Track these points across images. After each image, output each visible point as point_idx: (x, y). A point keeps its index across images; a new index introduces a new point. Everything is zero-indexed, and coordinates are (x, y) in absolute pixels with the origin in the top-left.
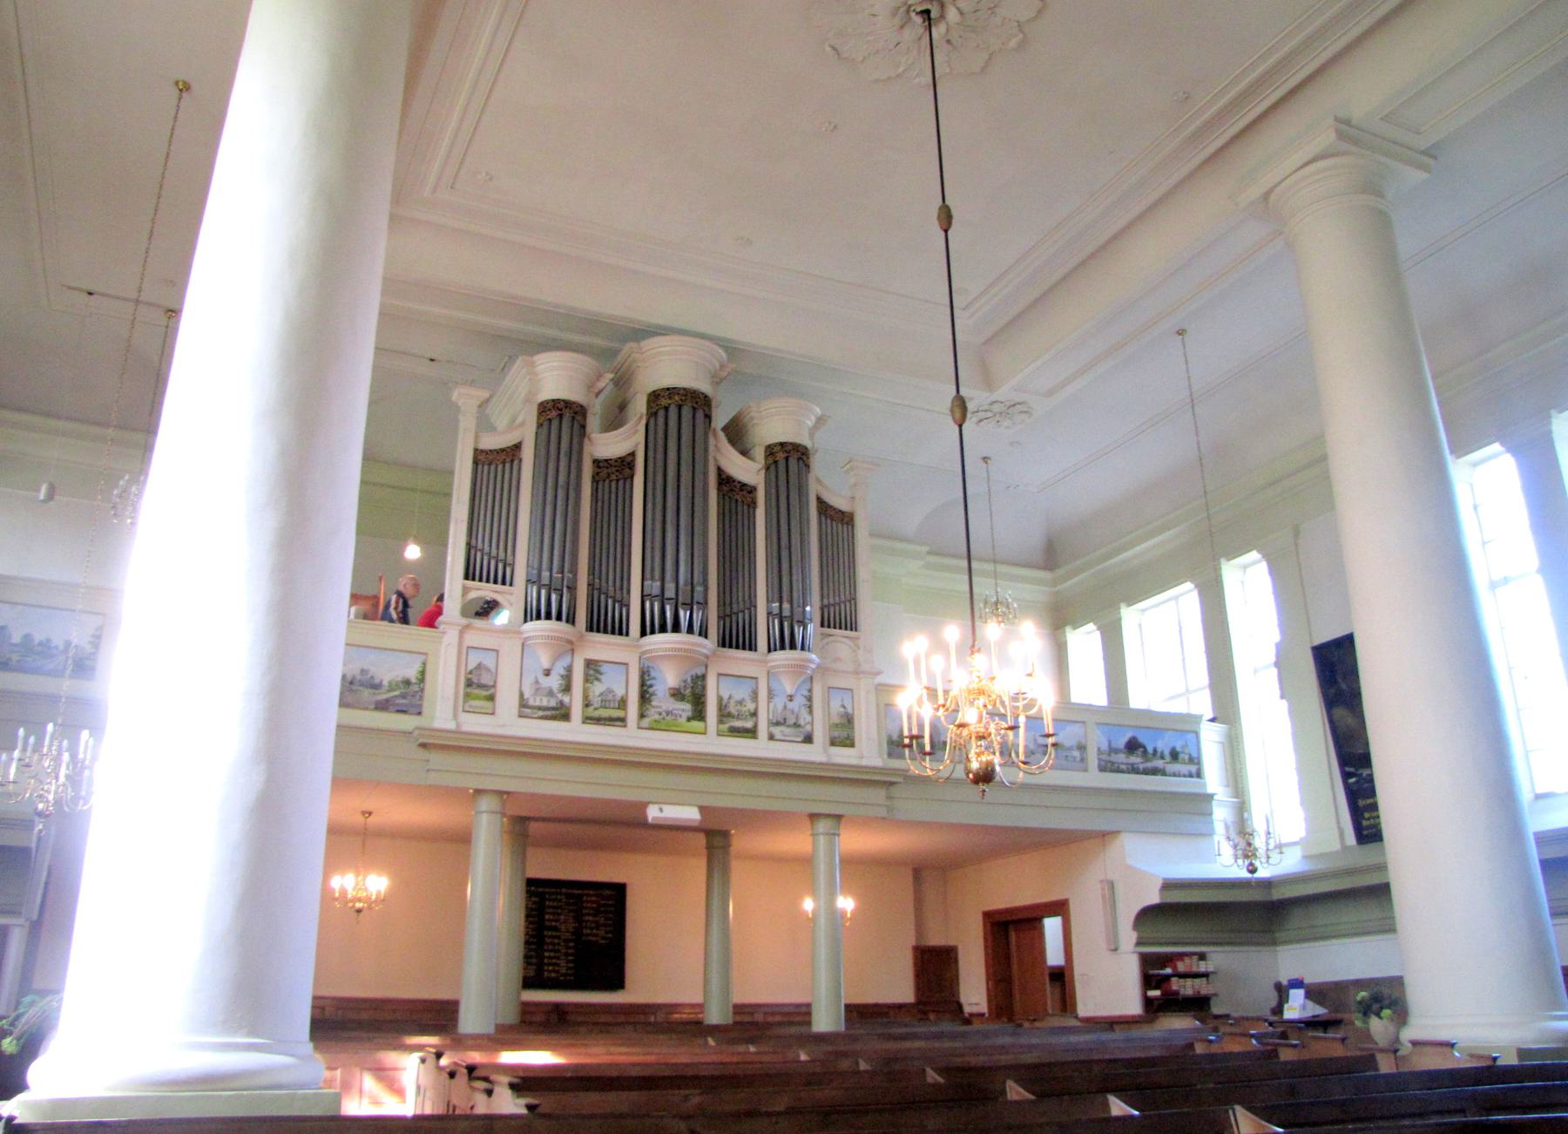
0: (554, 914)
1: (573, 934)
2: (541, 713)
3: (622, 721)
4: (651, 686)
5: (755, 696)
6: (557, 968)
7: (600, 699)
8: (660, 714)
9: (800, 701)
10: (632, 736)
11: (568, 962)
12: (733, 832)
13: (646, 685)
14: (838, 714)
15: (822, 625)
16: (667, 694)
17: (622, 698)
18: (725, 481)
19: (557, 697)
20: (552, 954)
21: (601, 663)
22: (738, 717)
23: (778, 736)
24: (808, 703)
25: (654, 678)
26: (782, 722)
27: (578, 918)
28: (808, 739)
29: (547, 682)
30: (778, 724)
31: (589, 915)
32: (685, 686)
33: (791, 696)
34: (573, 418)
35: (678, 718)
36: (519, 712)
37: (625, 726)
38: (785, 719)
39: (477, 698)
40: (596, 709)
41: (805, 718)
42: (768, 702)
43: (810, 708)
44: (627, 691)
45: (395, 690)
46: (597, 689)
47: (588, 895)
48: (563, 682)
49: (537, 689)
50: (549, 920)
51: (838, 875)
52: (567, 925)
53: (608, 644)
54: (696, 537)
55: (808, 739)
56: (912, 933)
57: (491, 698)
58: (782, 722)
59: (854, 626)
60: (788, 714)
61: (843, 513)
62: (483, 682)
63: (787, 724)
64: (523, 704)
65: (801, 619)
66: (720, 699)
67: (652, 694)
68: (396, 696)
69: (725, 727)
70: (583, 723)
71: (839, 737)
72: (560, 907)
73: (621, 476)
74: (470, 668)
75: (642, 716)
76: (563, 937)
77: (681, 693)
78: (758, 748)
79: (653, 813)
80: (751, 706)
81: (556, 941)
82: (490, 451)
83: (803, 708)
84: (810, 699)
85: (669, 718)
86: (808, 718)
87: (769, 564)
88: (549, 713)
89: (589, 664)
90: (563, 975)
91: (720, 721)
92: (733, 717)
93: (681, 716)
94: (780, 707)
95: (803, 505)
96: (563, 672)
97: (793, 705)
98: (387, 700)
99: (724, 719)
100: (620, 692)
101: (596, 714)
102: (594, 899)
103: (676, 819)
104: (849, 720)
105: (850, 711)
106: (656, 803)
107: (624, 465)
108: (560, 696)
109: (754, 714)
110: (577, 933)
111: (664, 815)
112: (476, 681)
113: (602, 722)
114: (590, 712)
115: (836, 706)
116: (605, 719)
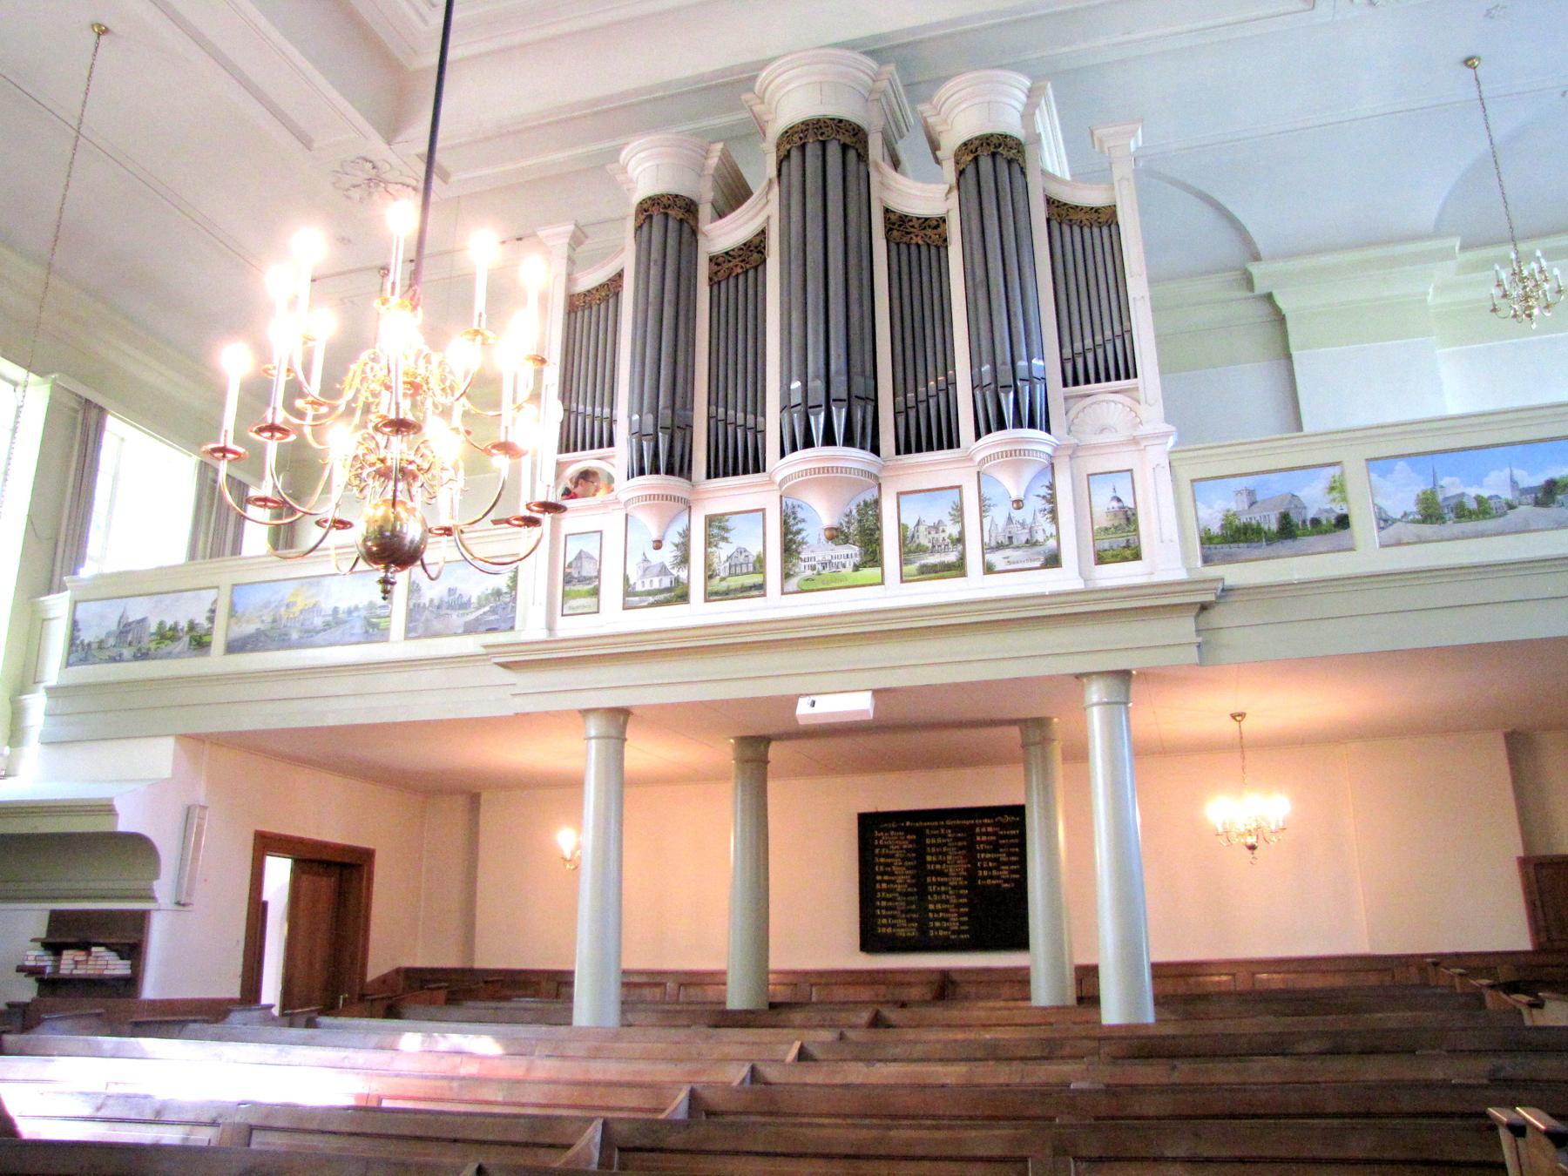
0: (937, 854)
1: (965, 878)
2: (651, 599)
3: (760, 588)
4: (799, 532)
5: (959, 513)
6: (945, 924)
7: (727, 564)
8: (813, 568)
9: (1035, 504)
10: (776, 605)
11: (960, 915)
12: (1056, 720)
13: (791, 533)
14: (1108, 512)
15: (1065, 385)
16: (823, 538)
17: (758, 556)
18: (898, 224)
19: (671, 574)
20: (939, 906)
21: (727, 517)
23: (1000, 565)
24: (1048, 506)
25: (803, 521)
26: (1006, 542)
27: (971, 856)
28: (1053, 561)
29: (656, 557)
30: (1000, 546)
31: (985, 851)
32: (848, 522)
34: (666, 215)
35: (841, 569)
37: (764, 595)
38: (1010, 538)
39: (579, 595)
40: (723, 579)
41: (1044, 526)
42: (981, 517)
43: (1053, 514)
44: (999, 572)
45: (484, 606)
46: (724, 551)
47: (981, 826)
48: (679, 553)
49: (645, 570)
50: (931, 863)
51: (1128, 770)
52: (956, 868)
53: (742, 487)
54: (682, 280)
55: (1053, 561)
56: (1518, 840)
57: (595, 592)
58: (1006, 542)
59: (1131, 371)
61: (1097, 210)
62: (584, 573)
64: (628, 591)
66: (902, 528)
67: (803, 543)
68: (485, 613)
69: (912, 568)
70: (706, 601)
71: (1112, 548)
72: (946, 844)
73: (748, 266)
75: (786, 576)
76: (899, 890)
77: (842, 532)
78: (973, 587)
79: (803, 708)
80: (953, 530)
81: (943, 889)
82: (589, 291)
83: (1039, 516)
84: (1051, 499)
85: (827, 571)
86: (1051, 529)
87: (1462, 422)
88: (661, 597)
89: (710, 521)
90: (954, 932)
91: (904, 562)
92: (925, 552)
93: (844, 566)
94: (1001, 521)
95: (1021, 213)
96: (677, 540)
97: (1023, 515)
98: (477, 619)
99: (912, 556)
100: (755, 549)
101: (723, 586)
102: (990, 829)
104: (1129, 518)
105: (1128, 503)
106: (807, 695)
107: (755, 249)
108: (674, 572)
109: (960, 540)
110: (972, 876)
111: (817, 709)
113: (731, 596)
114: (716, 584)
115: (1103, 503)
116: (736, 590)
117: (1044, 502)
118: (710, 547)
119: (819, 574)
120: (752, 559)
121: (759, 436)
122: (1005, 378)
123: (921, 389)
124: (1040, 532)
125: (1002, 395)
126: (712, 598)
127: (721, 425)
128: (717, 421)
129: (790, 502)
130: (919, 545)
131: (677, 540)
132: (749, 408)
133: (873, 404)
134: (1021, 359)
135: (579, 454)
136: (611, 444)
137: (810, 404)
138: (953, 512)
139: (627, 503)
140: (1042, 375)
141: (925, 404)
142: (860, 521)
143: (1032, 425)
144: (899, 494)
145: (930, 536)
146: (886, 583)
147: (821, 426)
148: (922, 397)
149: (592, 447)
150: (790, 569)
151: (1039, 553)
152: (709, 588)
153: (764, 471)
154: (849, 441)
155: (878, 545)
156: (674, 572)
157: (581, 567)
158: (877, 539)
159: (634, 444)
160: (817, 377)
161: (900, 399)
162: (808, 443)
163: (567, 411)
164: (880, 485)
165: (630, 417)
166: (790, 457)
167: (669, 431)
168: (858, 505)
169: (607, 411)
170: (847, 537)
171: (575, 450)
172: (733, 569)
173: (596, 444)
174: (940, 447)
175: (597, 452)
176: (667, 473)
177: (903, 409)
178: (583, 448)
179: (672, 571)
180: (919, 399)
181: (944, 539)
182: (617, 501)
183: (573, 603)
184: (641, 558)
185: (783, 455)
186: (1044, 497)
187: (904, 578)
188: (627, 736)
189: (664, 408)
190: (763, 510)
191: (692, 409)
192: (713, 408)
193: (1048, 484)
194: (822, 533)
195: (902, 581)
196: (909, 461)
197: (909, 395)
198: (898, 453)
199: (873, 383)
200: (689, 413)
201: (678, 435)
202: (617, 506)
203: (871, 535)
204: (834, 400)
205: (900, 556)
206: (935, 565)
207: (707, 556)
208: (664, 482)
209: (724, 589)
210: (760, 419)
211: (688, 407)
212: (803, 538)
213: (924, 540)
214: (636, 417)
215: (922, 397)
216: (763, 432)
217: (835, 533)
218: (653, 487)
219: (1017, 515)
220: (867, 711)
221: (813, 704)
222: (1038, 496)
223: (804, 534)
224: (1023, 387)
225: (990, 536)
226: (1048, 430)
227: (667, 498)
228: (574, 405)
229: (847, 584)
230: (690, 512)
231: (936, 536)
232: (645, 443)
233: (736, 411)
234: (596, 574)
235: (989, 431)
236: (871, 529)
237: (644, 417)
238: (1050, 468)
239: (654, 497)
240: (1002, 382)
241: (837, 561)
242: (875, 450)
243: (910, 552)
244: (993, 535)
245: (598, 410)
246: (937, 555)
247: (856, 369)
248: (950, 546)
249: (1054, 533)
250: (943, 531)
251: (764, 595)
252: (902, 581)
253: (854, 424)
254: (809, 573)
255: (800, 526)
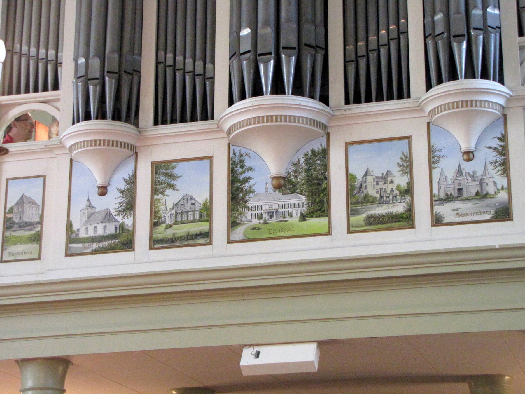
2: (95, 246)
4: (246, 180)
7: (173, 212)
8: (260, 217)
12: (507, 378)
13: (239, 181)
16: (270, 186)
17: (205, 205)
19: (116, 221)
21: (174, 164)
22: (381, 201)
24: (499, 159)
25: (251, 169)
26: (455, 194)
30: (449, 198)
32: (296, 172)
33: (468, 153)
35: (288, 218)
36: (67, 247)
37: (210, 244)
38: (460, 190)
39: (20, 241)
40: (170, 226)
57: (37, 238)
58: (455, 194)
60: (465, 181)
62: (26, 219)
63: (465, 195)
65: (499, 26)
66: (350, 178)
69: (359, 219)
70: (151, 248)
74: (9, 206)
75: (233, 224)
77: (290, 181)
80: (402, 181)
83: (490, 168)
85: (273, 220)
86: (502, 182)
88: (106, 243)
91: (351, 212)
92: (373, 202)
93: (291, 215)
94: (451, 173)
96: (123, 186)
99: (359, 207)
101: (169, 233)
103: (54, 280)
108: (119, 218)
109: (408, 191)
111: (263, 360)
112: (17, 220)
113: (177, 244)
114: (161, 232)
116: (181, 238)
117: (495, 154)
118: (155, 194)
119: (265, 223)
120: (198, 207)
121: (207, 83)
122: (459, 27)
123: (373, 38)
124: (491, 185)
125: (455, 45)
126: (157, 246)
127: (169, 71)
128: (165, 67)
129: (237, 150)
130: (366, 196)
131: (123, 186)
132: (198, 53)
133: (323, 52)
134: (475, 7)
135: (23, 96)
136: (56, 87)
137: (259, 52)
138: (401, 163)
139: (71, 148)
140: (498, 24)
141: (375, 54)
142: (307, 170)
143: (485, 76)
144: (347, 144)
145: (378, 187)
146: (333, 232)
147: (271, 74)
148: (373, 45)
149: (36, 90)
150: (236, 217)
151: (489, 206)
152: (154, 236)
153: (212, 118)
154: (298, 90)
155: (326, 195)
156: (119, 218)
157: (23, 212)
158: (325, 189)
159: (80, 89)
160: (266, 24)
161: (351, 48)
162: (257, 91)
163: (10, 51)
164: (328, 134)
165: (76, 60)
166: (238, 105)
167: (117, 75)
168: (306, 155)
169: (52, 53)
170: (294, 186)
171: (18, 92)
172: (179, 216)
173: (445, 75)
174: (390, 97)
175: (41, 95)
176: (113, 118)
177: (353, 58)
178: (27, 91)
179: (116, 217)
180: (370, 48)
181: (392, 190)
182: (61, 146)
183: (13, 249)
184: (85, 203)
185: (231, 103)
186: (495, 149)
187: (351, 229)
188: (66, 388)
189: (112, 51)
190: (210, 158)
191: (140, 54)
192: (162, 53)
193: (500, 136)
194: (269, 181)
195: (349, 232)
196: (357, 111)
197: (359, 44)
198: (347, 102)
199: (323, 31)
200: (136, 57)
201: (126, 78)
202: (62, 151)
203: (319, 184)
204: (284, 48)
205: (348, 207)
206: (382, 216)
207: (153, 203)
208: (110, 127)
209: (171, 236)
210: (209, 66)
211: (136, 51)
212: (250, 187)
213: (372, 191)
214: (82, 60)
215: (373, 45)
216: (212, 78)
217: (282, 182)
218: (104, 132)
219: (468, 167)
220: (312, 362)
221: (257, 355)
222: (490, 148)
223: (251, 182)
224: (477, 37)
225: (439, 188)
226: (501, 81)
227: (113, 143)
228: (17, 46)
229: (294, 233)
230: (137, 156)
231: (384, 187)
232: (91, 88)
233: (185, 59)
234: (38, 220)
235: (440, 81)
236: (318, 179)
237: (90, 61)
238: (502, 120)
239: (100, 142)
240: (454, 31)
241: (284, 210)
242: (325, 99)
243: (357, 202)
244: (443, 187)
245: (42, 51)
246: (385, 206)
247: (307, 14)
248: (398, 197)
249: (506, 186)
250: (392, 182)
251: (210, 244)
252: (349, 232)
253: (304, 75)
254: (255, 222)
255: (247, 174)
